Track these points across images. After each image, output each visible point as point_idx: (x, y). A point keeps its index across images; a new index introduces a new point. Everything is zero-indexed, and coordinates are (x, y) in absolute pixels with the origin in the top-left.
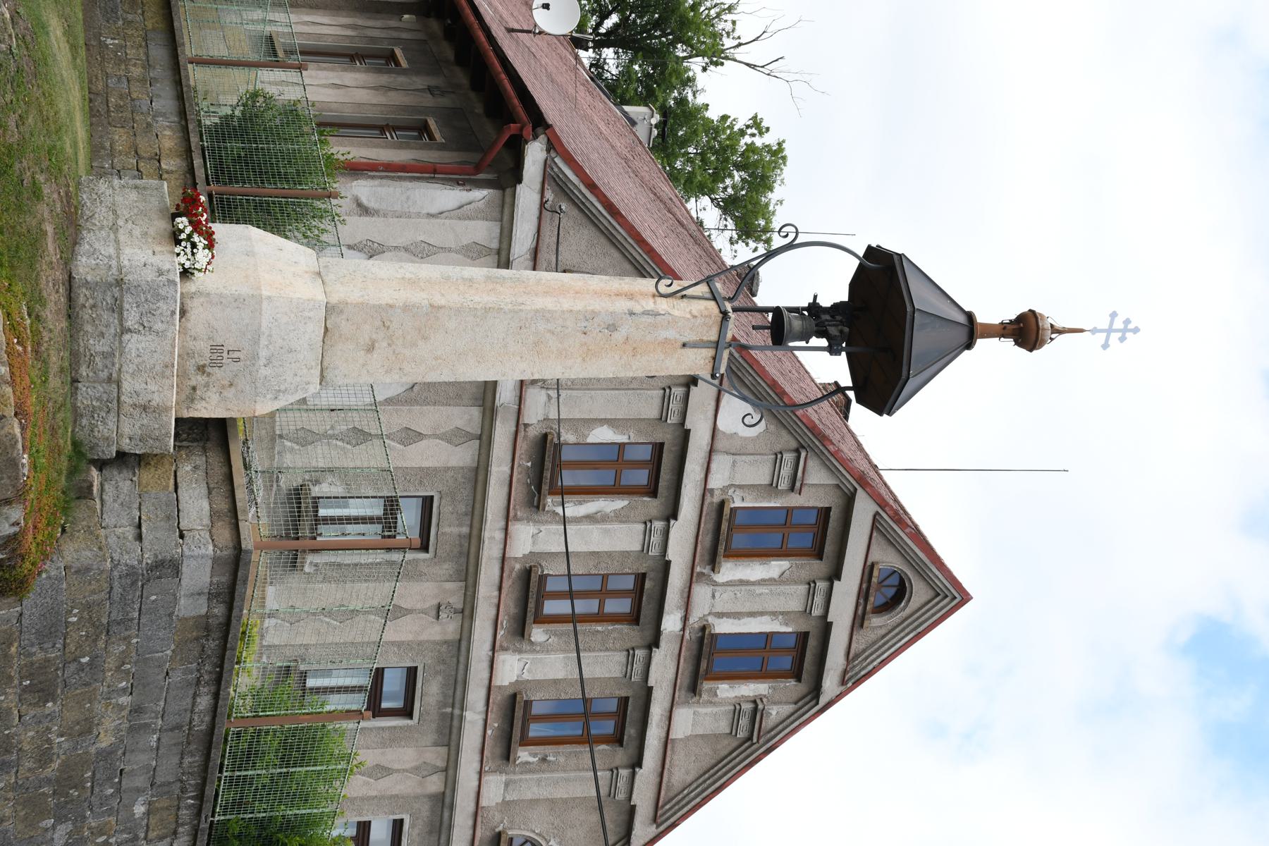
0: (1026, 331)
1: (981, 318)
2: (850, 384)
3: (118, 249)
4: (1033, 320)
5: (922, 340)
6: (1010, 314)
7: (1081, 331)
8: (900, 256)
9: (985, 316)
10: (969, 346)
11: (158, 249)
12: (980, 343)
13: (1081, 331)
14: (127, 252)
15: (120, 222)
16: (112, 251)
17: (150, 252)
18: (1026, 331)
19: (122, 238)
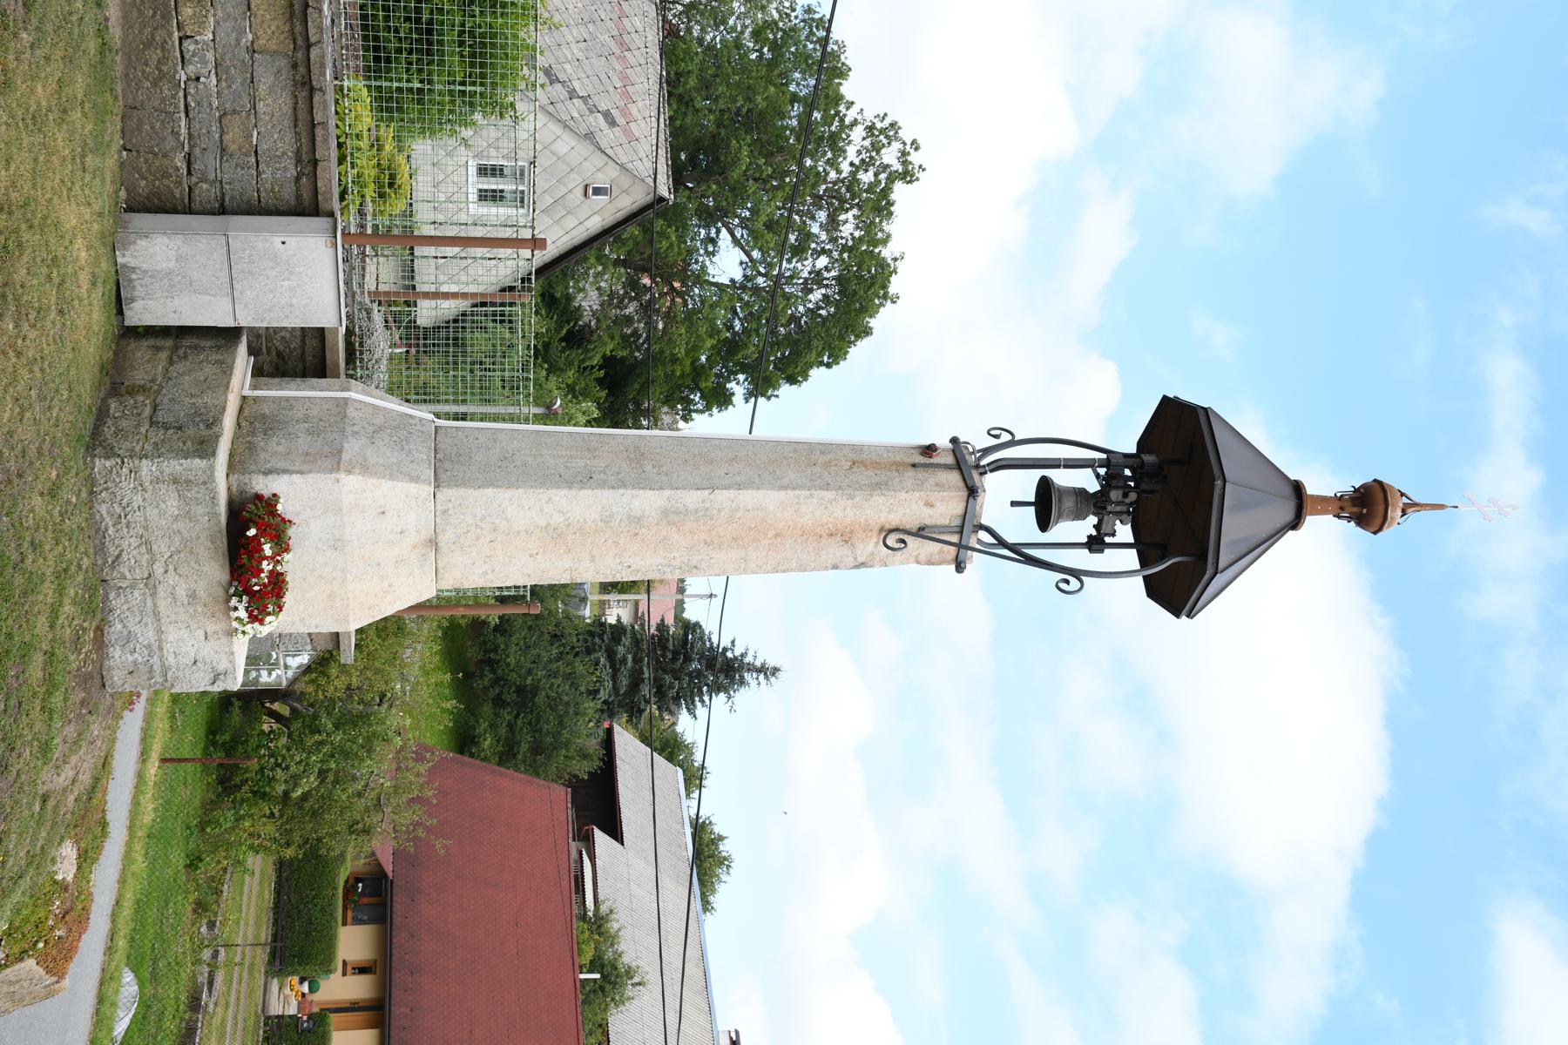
0: (1368, 506)
1: (1311, 489)
2: (1132, 540)
3: (159, 632)
4: (1380, 495)
5: (1234, 526)
6: (1344, 484)
7: (1442, 507)
8: (1206, 410)
9: (1318, 485)
10: (1295, 524)
11: (211, 627)
12: (1311, 521)
13: (1442, 507)
14: (172, 635)
15: (158, 569)
16: (151, 635)
17: (201, 633)
18: (1368, 506)
19: (163, 605)
